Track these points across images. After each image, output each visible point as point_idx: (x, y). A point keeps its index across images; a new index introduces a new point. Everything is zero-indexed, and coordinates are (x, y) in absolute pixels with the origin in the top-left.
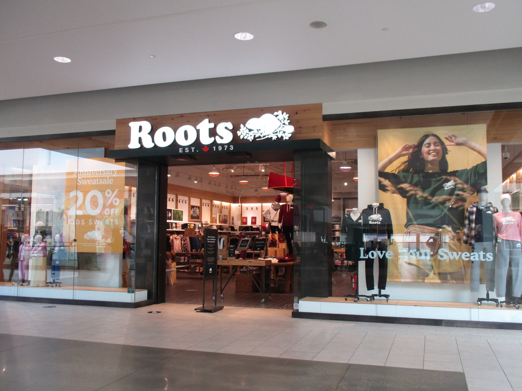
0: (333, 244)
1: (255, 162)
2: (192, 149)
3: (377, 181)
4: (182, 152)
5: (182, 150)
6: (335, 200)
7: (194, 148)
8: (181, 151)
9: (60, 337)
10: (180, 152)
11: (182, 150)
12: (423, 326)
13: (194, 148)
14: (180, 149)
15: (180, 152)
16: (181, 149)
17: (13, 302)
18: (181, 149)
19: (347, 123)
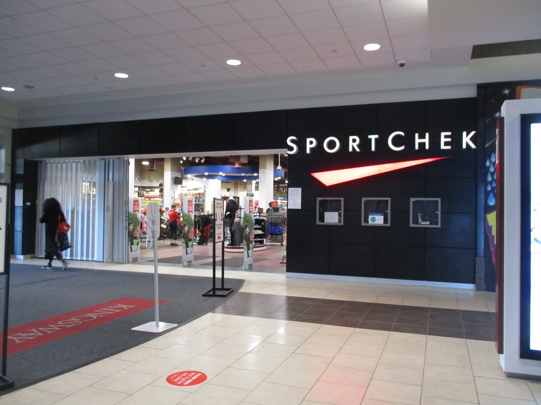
0: (237, 199)
1: (268, 154)
2: (371, 139)
3: (235, 242)
4: (449, 147)
5: (449, 140)
6: (248, 180)
7: (377, 136)
8: (446, 144)
9: (203, 373)
10: (443, 147)
11: (449, 140)
12: (199, 269)
13: (377, 136)
14: (443, 134)
15: (443, 147)
16: (446, 137)
17: (255, 156)
18: (446, 137)
19: (161, 165)
